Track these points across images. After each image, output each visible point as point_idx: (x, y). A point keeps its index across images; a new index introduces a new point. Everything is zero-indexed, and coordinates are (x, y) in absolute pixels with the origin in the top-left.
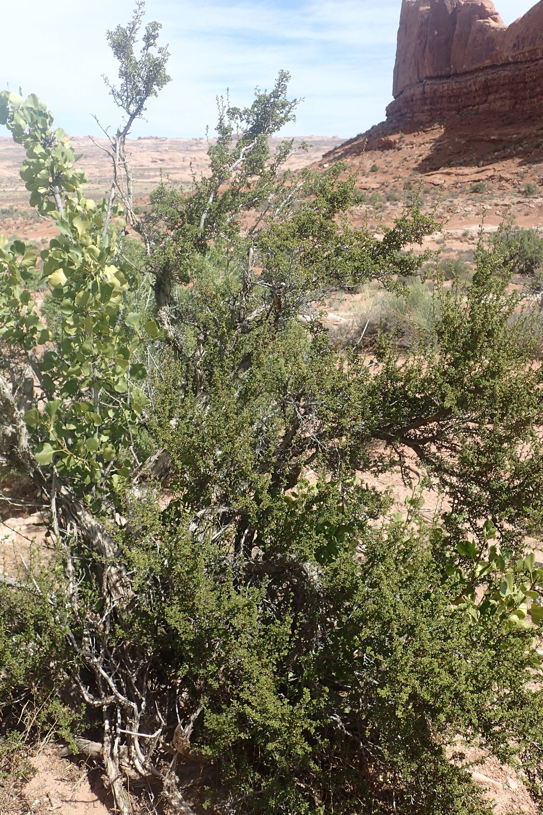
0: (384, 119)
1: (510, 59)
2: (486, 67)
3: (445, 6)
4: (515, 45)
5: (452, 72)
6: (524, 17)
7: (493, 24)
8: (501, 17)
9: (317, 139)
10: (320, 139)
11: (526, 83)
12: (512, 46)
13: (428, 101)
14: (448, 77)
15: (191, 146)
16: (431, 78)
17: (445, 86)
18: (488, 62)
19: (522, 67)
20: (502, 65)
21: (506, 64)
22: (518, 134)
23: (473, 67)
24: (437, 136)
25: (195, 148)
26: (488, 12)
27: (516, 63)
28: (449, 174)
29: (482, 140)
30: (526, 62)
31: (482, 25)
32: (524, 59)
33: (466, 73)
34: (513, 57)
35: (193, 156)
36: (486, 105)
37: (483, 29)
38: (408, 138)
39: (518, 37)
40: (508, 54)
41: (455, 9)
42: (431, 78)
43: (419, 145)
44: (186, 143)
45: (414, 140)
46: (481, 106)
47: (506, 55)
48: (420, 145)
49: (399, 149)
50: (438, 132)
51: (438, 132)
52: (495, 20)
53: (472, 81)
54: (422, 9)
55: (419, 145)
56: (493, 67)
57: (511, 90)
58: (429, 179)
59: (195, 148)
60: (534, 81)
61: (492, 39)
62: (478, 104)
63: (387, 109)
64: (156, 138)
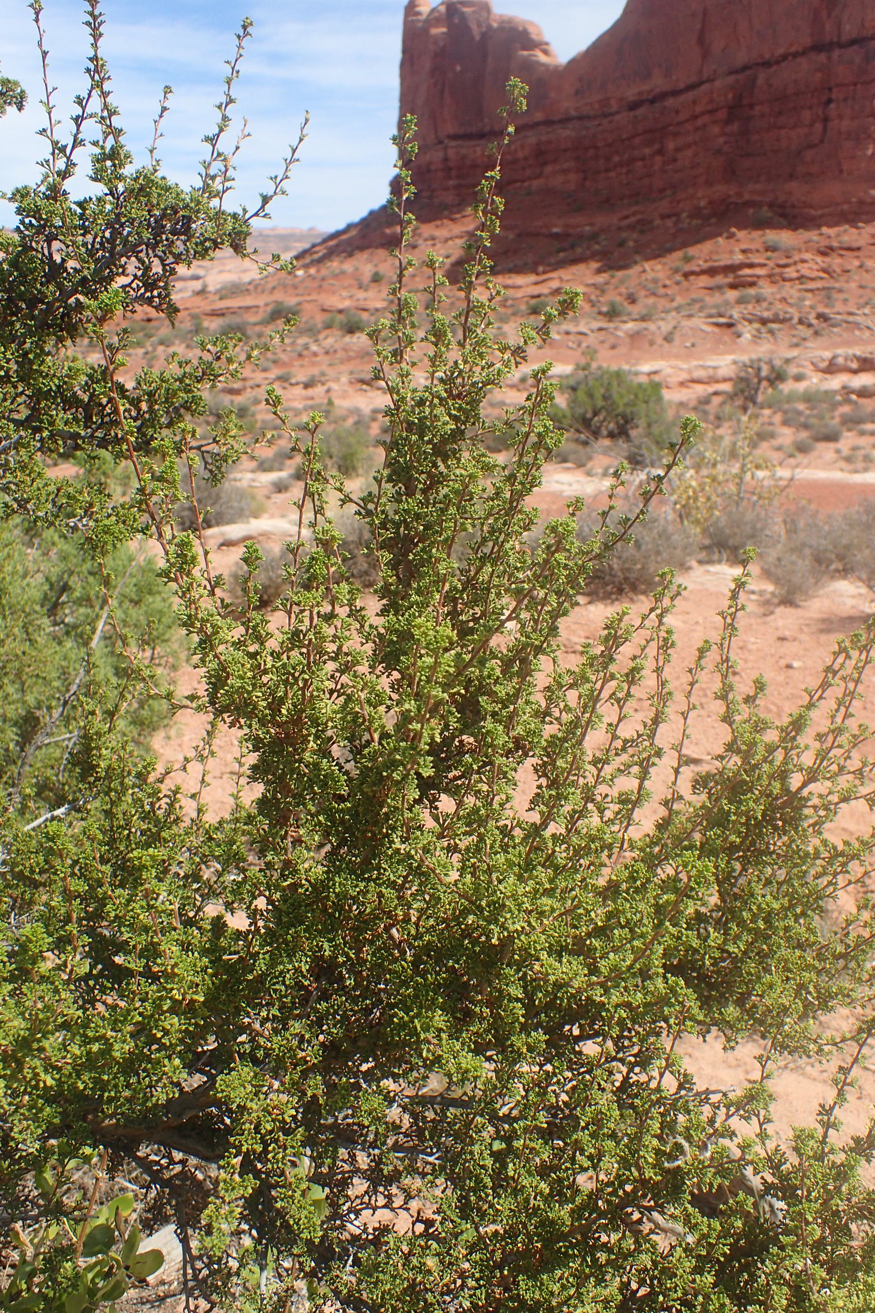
1: (573, 113)
2: (538, 124)
3: (468, 28)
4: (577, 93)
7: (543, 58)
9: (283, 232)
13: (453, 173)
21: (566, 120)
22: (591, 225)
26: (532, 41)
27: (580, 118)
36: (541, 181)
40: (568, 105)
45: (437, 233)
48: (446, 240)
52: (546, 52)
56: (548, 123)
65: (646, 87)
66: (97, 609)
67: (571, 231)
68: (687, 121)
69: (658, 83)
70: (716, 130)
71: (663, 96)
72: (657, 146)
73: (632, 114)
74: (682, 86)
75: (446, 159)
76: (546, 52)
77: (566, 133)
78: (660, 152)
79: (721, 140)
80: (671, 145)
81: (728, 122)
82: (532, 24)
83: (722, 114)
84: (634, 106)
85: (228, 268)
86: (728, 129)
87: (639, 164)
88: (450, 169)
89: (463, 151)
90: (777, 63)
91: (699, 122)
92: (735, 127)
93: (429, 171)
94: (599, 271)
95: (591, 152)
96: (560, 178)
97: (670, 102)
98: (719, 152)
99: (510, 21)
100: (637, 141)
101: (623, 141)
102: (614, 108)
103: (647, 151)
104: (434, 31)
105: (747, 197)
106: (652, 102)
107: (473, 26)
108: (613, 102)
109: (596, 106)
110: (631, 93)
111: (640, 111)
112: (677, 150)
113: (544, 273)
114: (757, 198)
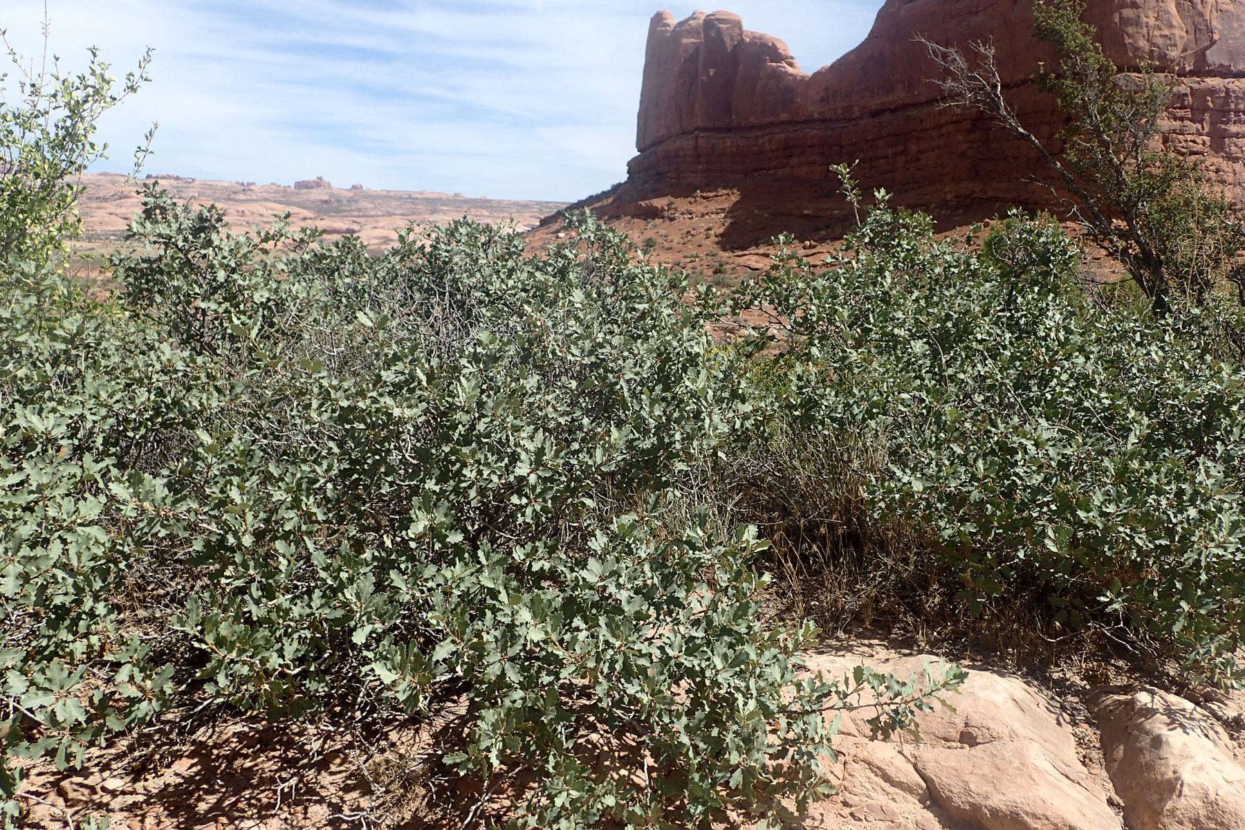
0: (624, 177)
1: (816, 115)
2: (783, 123)
3: (723, 41)
4: (822, 99)
5: (735, 124)
6: (833, 66)
7: (790, 70)
8: (796, 62)
9: (431, 196)
10: (436, 196)
11: (842, 147)
12: (818, 98)
13: (703, 159)
14: (728, 130)
15: (235, 193)
16: (704, 129)
17: (728, 142)
18: (784, 116)
19: (834, 126)
20: (805, 121)
21: (810, 121)
22: (841, 209)
23: (765, 121)
24: (726, 205)
25: (242, 197)
26: (780, 54)
27: (824, 120)
28: (767, 256)
29: (790, 215)
30: (837, 120)
31: (774, 70)
32: (834, 117)
33: (752, 127)
34: (820, 113)
35: (241, 208)
36: (787, 170)
37: (778, 76)
38: (681, 204)
39: (826, 88)
40: (815, 110)
41: (735, 47)
42: (704, 129)
43: (707, 214)
44: (227, 188)
45: (693, 208)
46: (781, 171)
47: (810, 109)
48: (703, 216)
49: (672, 219)
50: (728, 198)
51: (728, 198)
52: (791, 65)
53: (766, 138)
54: (685, 41)
55: (707, 214)
56: (792, 123)
57: (822, 154)
58: (741, 260)
59: (242, 197)
60: (853, 145)
61: (788, 90)
62: (775, 168)
63: (629, 164)
64: (177, 178)
65: (890, 99)
66: (468, 572)
67: (821, 214)
68: (932, 129)
69: (900, 95)
70: (960, 138)
71: (904, 107)
72: (900, 148)
73: (876, 120)
74: (923, 99)
75: (696, 147)
76: (791, 65)
77: (812, 132)
78: (903, 153)
79: (965, 146)
80: (913, 147)
81: (971, 132)
82: (779, 41)
83: (967, 125)
84: (875, 114)
85: (381, 224)
86: (971, 137)
87: (882, 161)
88: (700, 156)
89: (714, 141)
90: (1016, 85)
91: (944, 130)
92: (978, 135)
93: (677, 156)
94: (737, 237)
95: (836, 149)
96: (805, 169)
97: (914, 112)
98: (962, 155)
99: (761, 37)
100: (881, 142)
101: (867, 141)
102: (857, 114)
103: (890, 151)
104: (685, 41)
105: (990, 193)
106: (893, 111)
107: (727, 40)
108: (856, 109)
109: (840, 111)
110: (874, 103)
111: (884, 118)
112: (919, 152)
113: (811, 247)
114: (1000, 195)
